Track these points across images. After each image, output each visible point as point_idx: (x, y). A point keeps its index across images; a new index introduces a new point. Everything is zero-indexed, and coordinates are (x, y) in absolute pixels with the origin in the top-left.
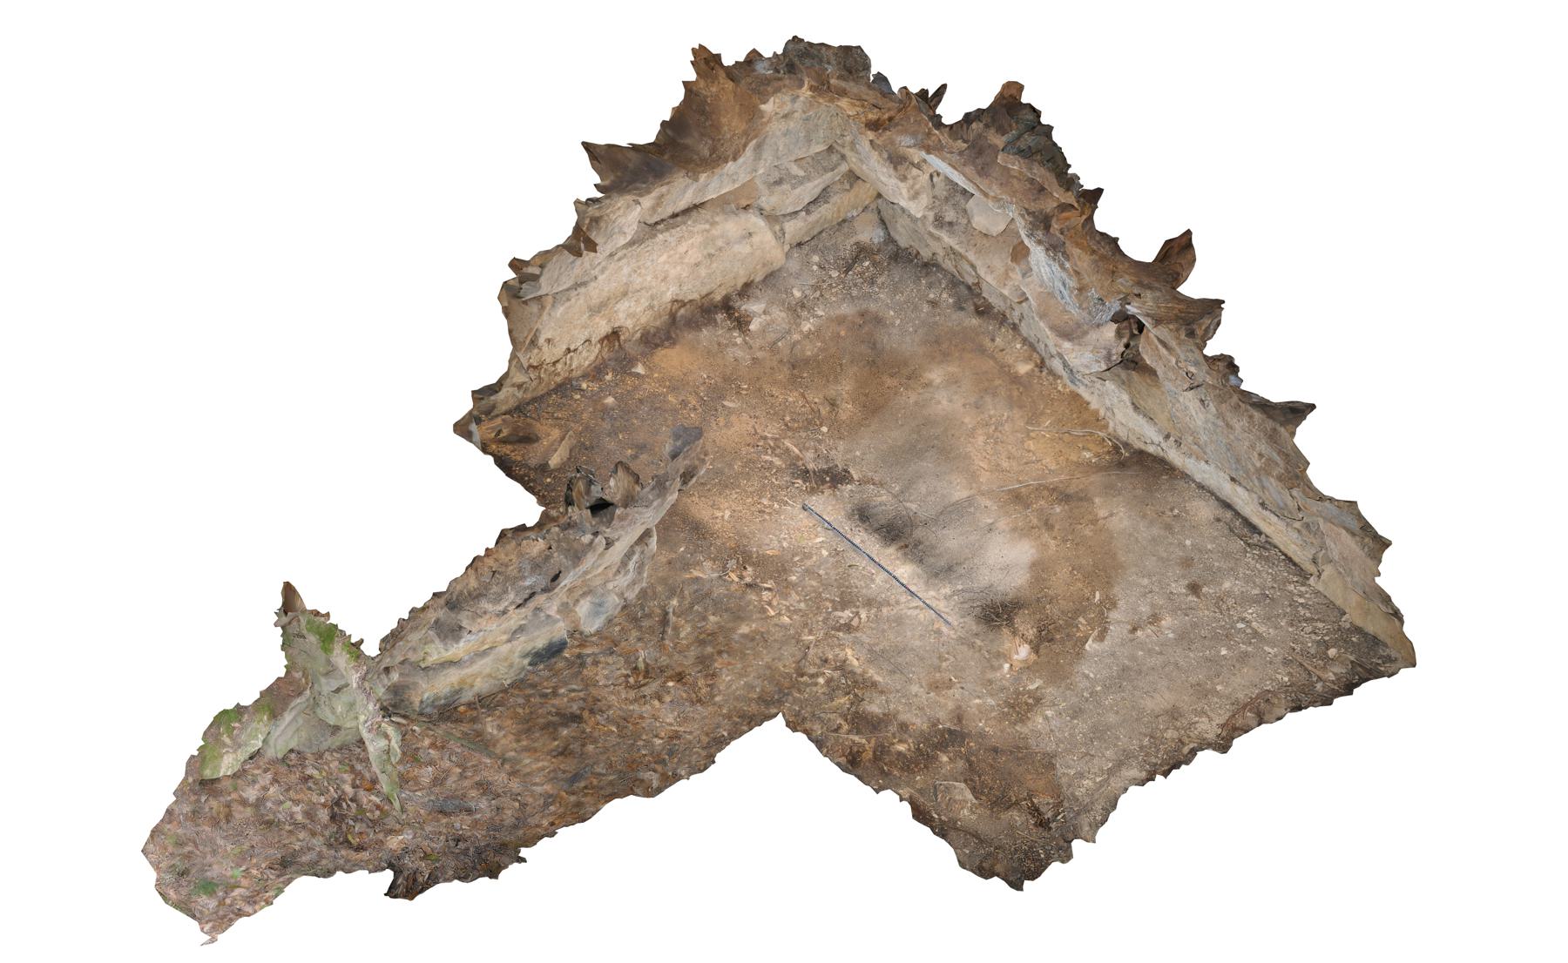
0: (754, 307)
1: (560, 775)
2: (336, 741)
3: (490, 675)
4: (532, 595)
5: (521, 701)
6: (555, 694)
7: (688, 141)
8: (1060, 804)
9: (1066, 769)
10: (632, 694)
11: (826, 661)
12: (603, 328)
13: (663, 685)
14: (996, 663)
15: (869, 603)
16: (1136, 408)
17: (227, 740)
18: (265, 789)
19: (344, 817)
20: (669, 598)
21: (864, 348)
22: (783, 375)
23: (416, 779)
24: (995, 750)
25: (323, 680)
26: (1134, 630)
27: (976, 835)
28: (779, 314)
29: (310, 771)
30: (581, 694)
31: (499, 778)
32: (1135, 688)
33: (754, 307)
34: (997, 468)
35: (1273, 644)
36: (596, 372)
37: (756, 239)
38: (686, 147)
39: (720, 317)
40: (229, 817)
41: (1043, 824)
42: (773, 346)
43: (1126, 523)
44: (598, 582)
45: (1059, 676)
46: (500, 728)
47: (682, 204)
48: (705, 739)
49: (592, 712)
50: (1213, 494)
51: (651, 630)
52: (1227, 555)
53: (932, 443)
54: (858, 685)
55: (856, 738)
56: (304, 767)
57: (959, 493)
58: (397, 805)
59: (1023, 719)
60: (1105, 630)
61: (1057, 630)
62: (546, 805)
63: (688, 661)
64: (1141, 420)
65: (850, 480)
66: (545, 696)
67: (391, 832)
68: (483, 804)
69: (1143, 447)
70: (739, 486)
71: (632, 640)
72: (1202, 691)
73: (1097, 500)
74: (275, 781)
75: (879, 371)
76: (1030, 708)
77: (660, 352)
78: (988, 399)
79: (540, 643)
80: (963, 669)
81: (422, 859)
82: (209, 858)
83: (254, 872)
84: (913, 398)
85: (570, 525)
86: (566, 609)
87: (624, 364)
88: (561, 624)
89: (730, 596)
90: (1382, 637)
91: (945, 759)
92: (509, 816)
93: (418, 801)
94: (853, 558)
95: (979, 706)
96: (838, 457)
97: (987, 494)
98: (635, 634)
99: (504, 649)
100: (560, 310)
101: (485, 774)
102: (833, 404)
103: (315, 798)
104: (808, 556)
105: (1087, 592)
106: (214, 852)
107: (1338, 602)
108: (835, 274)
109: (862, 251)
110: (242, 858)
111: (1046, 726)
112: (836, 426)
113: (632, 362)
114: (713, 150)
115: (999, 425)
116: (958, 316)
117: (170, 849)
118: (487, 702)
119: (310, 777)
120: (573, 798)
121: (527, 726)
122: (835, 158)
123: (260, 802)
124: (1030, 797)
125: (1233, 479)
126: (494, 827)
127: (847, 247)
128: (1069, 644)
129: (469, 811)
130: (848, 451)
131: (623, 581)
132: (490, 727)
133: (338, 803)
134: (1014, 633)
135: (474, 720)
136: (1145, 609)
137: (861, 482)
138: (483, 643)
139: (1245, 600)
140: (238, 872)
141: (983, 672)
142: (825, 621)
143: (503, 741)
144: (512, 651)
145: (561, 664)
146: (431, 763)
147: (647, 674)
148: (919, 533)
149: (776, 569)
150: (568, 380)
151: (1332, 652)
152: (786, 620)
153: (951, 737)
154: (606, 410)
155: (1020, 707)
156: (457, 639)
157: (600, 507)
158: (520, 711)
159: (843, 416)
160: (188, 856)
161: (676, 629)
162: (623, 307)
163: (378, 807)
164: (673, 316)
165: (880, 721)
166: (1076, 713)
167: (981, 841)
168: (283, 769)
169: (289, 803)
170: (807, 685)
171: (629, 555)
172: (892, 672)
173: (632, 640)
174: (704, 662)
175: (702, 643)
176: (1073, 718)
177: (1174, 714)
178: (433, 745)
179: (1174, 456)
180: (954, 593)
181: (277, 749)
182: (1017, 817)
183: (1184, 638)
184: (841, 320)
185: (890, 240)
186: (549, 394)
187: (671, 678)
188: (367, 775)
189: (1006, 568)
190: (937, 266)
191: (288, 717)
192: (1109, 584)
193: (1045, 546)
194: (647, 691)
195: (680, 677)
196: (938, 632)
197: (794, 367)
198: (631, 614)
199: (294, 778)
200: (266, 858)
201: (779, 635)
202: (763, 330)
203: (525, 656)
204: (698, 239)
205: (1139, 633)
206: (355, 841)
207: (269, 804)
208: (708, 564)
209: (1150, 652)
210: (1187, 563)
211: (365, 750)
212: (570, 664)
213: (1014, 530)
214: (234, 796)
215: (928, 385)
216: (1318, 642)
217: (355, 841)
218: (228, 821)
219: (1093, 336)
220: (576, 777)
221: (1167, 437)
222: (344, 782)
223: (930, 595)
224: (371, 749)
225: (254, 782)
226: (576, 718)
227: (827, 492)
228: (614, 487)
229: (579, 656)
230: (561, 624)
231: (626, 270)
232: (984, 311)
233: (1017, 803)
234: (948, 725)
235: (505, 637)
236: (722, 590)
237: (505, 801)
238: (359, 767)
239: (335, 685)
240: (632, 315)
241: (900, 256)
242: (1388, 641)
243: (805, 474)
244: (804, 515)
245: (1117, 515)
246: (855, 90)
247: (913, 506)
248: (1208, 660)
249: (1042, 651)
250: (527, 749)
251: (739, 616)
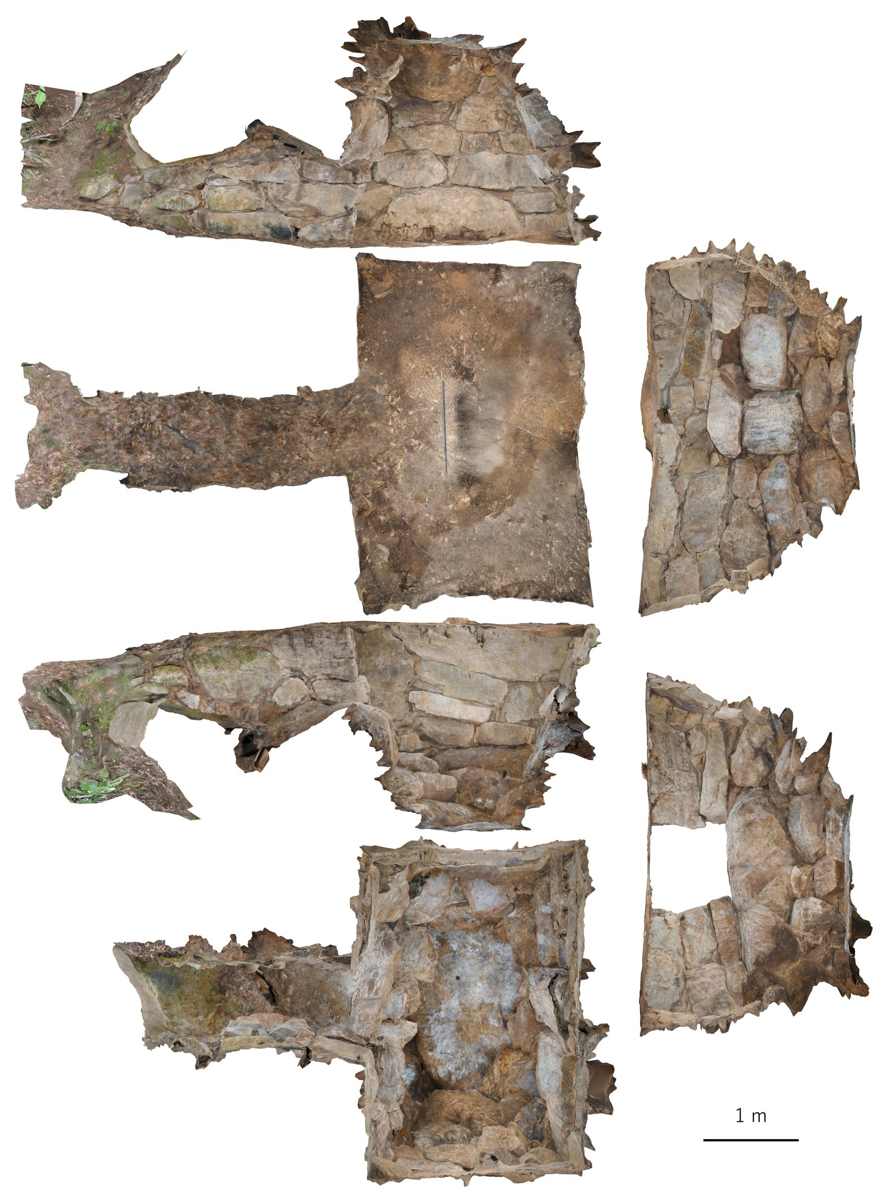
1: (244, 455)
6: (278, 411)
8: (416, 582)
11: (388, 460)
14: (448, 502)
20: (358, 393)
21: (525, 324)
26: (510, 520)
28: (512, 285)
30: (288, 417)
32: (487, 548)
35: (552, 561)
41: (403, 587)
42: (497, 299)
43: (540, 477)
46: (242, 417)
52: (567, 513)
53: (505, 387)
54: (390, 478)
55: (369, 503)
57: (499, 418)
59: (436, 534)
60: (499, 514)
62: (226, 466)
66: (273, 410)
70: (430, 355)
71: (329, 403)
72: (509, 566)
73: (538, 460)
76: (444, 531)
77: (457, 273)
80: (434, 497)
82: (63, 429)
91: (392, 534)
98: (332, 401)
104: (425, 406)
108: (547, 281)
116: (566, 336)
120: (237, 470)
129: (194, 452)
130: (482, 366)
136: (521, 514)
139: (559, 535)
141: (441, 503)
143: (238, 424)
148: (472, 423)
151: (571, 579)
153: (401, 525)
154: (416, 285)
155: (440, 528)
158: (256, 413)
159: (495, 348)
160: (55, 424)
161: (349, 409)
166: (457, 545)
167: (374, 580)
170: (373, 467)
175: (353, 420)
176: (454, 546)
177: (491, 569)
178: (209, 411)
180: (461, 460)
182: (396, 578)
183: (524, 537)
184: (529, 305)
192: (517, 495)
193: (508, 463)
194: (315, 430)
195: (332, 431)
196: (439, 474)
197: (498, 312)
201: (383, 436)
202: (500, 288)
205: (510, 523)
210: (550, 506)
213: (503, 448)
215: (527, 362)
216: (570, 571)
220: (248, 460)
222: (154, 414)
223: (451, 454)
225: (108, 405)
226: (274, 429)
227: (459, 379)
234: (406, 520)
248: (523, 553)
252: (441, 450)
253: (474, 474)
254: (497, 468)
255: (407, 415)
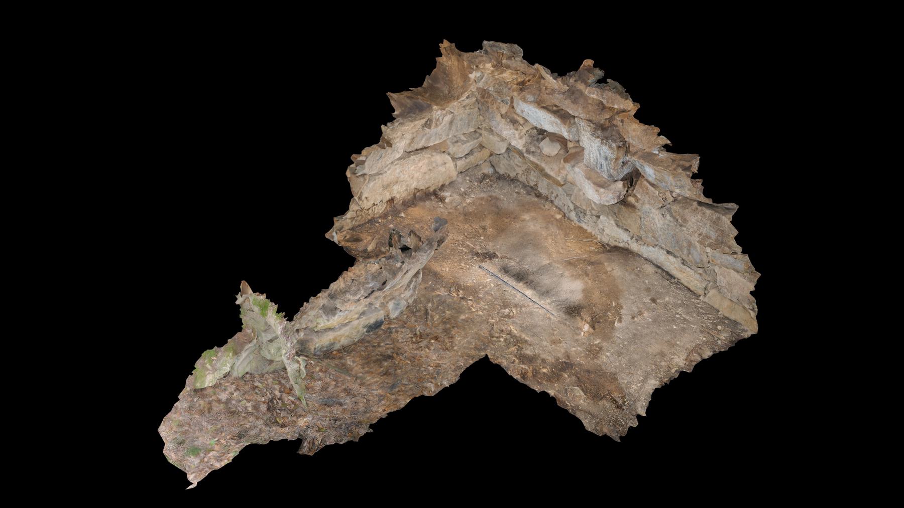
0: (446, 194)
1: (385, 385)
2: (271, 368)
3: (348, 336)
4: (373, 292)
5: (363, 349)
6: (379, 346)
7: (438, 85)
9: (623, 379)
10: (415, 346)
12: (388, 197)
13: (429, 342)
15: (516, 306)
16: (618, 226)
17: (209, 367)
18: (232, 394)
19: (274, 408)
22: (461, 218)
23: (312, 388)
24: (588, 371)
25: (263, 334)
26: (633, 318)
27: (590, 413)
28: (456, 197)
29: (257, 384)
31: (355, 387)
33: (446, 194)
34: (558, 252)
36: (384, 216)
37: (447, 165)
38: (438, 89)
39: (433, 197)
40: (210, 410)
43: (620, 273)
44: (397, 293)
45: (606, 337)
46: (354, 362)
47: (420, 146)
48: (453, 367)
49: (397, 354)
50: (651, 262)
51: (421, 317)
52: (664, 287)
53: (529, 242)
54: (519, 342)
55: (523, 366)
56: (253, 381)
57: (545, 262)
58: (304, 402)
61: (600, 317)
62: (380, 400)
63: (439, 331)
64: (620, 231)
65: (497, 257)
66: (374, 346)
67: (300, 416)
68: (348, 400)
69: (617, 244)
71: (413, 321)
74: (237, 389)
75: (502, 219)
77: (410, 209)
78: (550, 225)
79: (372, 321)
81: (317, 431)
83: (223, 441)
84: (518, 226)
85: (391, 257)
86: (383, 305)
87: (396, 213)
88: (382, 312)
89: (454, 303)
90: (739, 321)
92: (361, 407)
93: (314, 399)
94: (505, 287)
95: (575, 351)
96: (490, 247)
97: (558, 262)
98: (413, 319)
99: (355, 323)
100: (372, 184)
101: (348, 384)
102: (484, 228)
103: (259, 398)
104: (486, 286)
105: (609, 302)
106: (200, 430)
107: (716, 306)
109: (485, 176)
110: (216, 433)
111: (607, 359)
112: (486, 236)
113: (399, 212)
114: (450, 92)
115: (556, 236)
116: (529, 197)
117: (175, 429)
118: (346, 350)
119: (257, 387)
120: (393, 397)
121: (367, 361)
122: (478, 135)
123: (228, 401)
124: (610, 394)
125: (668, 252)
126: (354, 412)
127: (479, 175)
128: (607, 324)
129: (341, 404)
131: (408, 294)
132: (349, 361)
133: (271, 401)
134: (582, 319)
135: (341, 358)
137: (502, 258)
138: (346, 318)
139: (676, 305)
140: (213, 442)
142: (498, 313)
144: (359, 324)
145: (380, 332)
146: (320, 379)
147: (421, 337)
148: (531, 277)
149: (472, 291)
150: (373, 218)
152: (480, 313)
155: (594, 352)
156: (334, 315)
157: (405, 249)
160: (185, 433)
161: (432, 316)
162: (396, 187)
163: (293, 403)
164: (415, 195)
165: (533, 358)
167: (593, 416)
168: (242, 383)
169: (244, 401)
171: (410, 282)
172: (533, 336)
173: (413, 321)
174: (446, 331)
177: (662, 355)
178: (321, 370)
179: (634, 247)
180: (552, 302)
181: (238, 372)
182: (606, 404)
183: (655, 321)
184: (482, 199)
185: (496, 172)
186: (365, 223)
187: (432, 339)
188: (288, 386)
189: (572, 292)
190: (518, 180)
191: (244, 355)
193: (587, 282)
194: (422, 344)
195: (436, 338)
196: (549, 318)
198: (411, 310)
199: (248, 387)
200: (230, 433)
201: (479, 320)
202: (451, 202)
203: (365, 327)
204: (426, 161)
206: (280, 421)
207: (233, 402)
208: (442, 289)
209: (643, 327)
211: (286, 373)
212: (385, 332)
213: (572, 276)
214: (214, 398)
215: (524, 220)
217: (280, 421)
218: (209, 412)
219: (613, 186)
220: (393, 386)
221: (632, 238)
224: (289, 369)
225: (225, 390)
226: (390, 357)
228: (409, 241)
229: (389, 328)
230: (382, 312)
231: (398, 171)
232: (539, 195)
233: (604, 397)
235: (357, 316)
236: (450, 300)
237: (359, 398)
238: (283, 382)
239: (270, 337)
240: (400, 192)
241: (500, 177)
242: (743, 323)
243: (477, 254)
244: (480, 270)
245: (615, 269)
246: (514, 65)
247: (527, 267)
249: (596, 327)
250: (367, 372)
251: (459, 311)
252: (531, 304)
253: (572, 304)
254: (584, 290)
255: (479, 298)
